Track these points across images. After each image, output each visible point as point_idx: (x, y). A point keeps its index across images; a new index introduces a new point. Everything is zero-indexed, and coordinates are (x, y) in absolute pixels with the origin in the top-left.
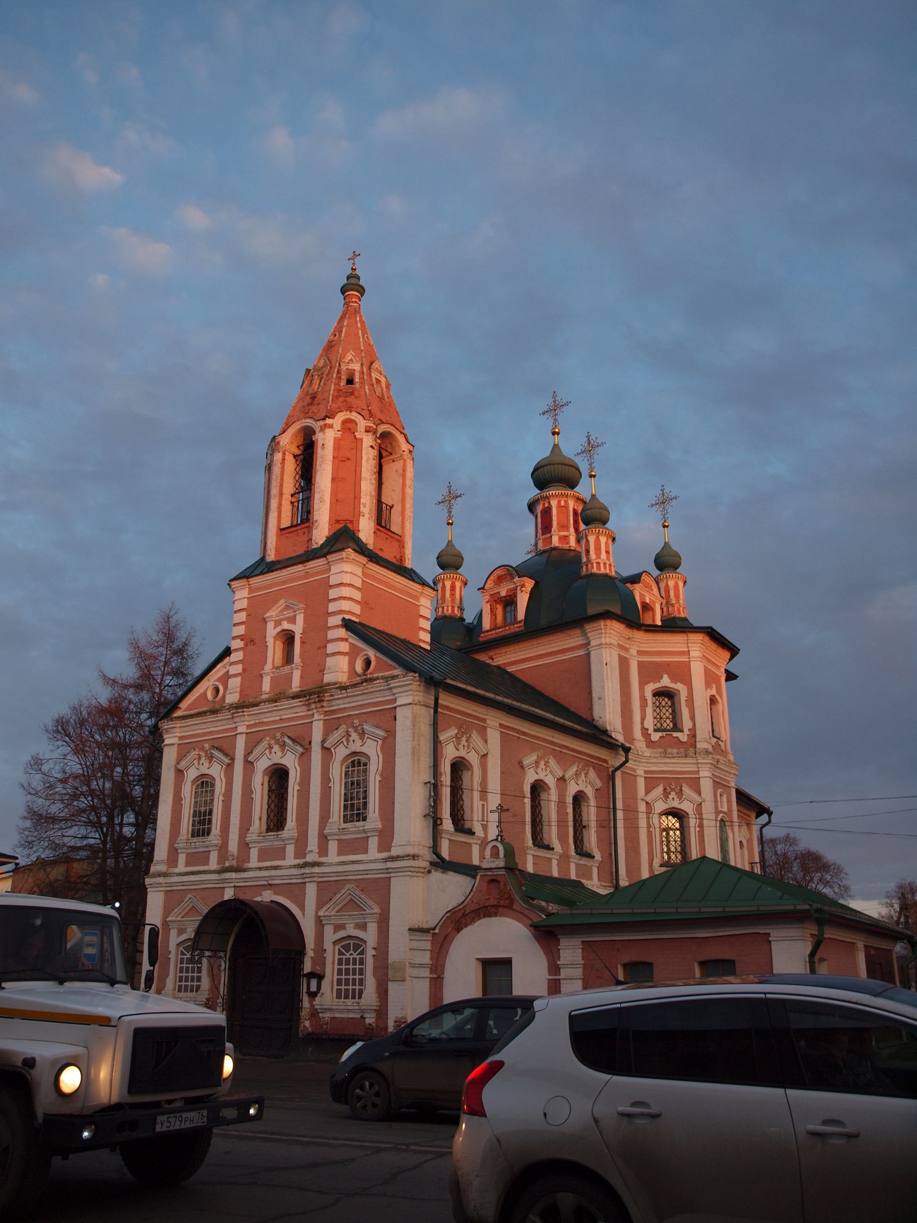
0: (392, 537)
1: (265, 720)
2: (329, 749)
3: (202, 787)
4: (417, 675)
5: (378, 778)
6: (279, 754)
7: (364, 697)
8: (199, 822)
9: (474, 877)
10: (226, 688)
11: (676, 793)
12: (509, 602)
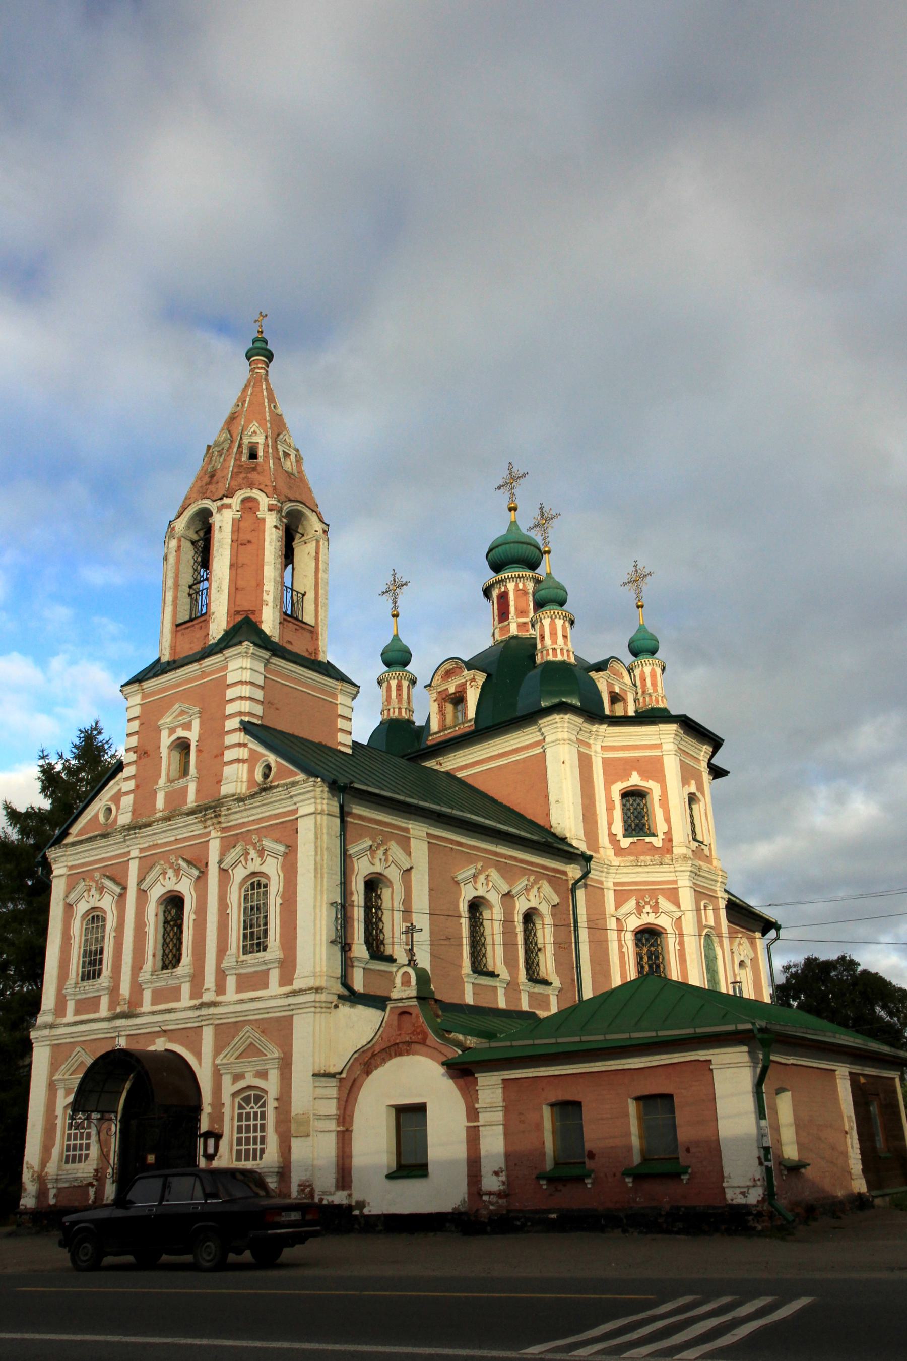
0: (302, 628)
1: (159, 842)
2: (226, 870)
3: (93, 923)
4: (319, 779)
5: (279, 901)
6: (174, 879)
7: (264, 808)
8: (90, 963)
9: (384, 1010)
10: (118, 808)
11: (651, 907)
12: (458, 699)
